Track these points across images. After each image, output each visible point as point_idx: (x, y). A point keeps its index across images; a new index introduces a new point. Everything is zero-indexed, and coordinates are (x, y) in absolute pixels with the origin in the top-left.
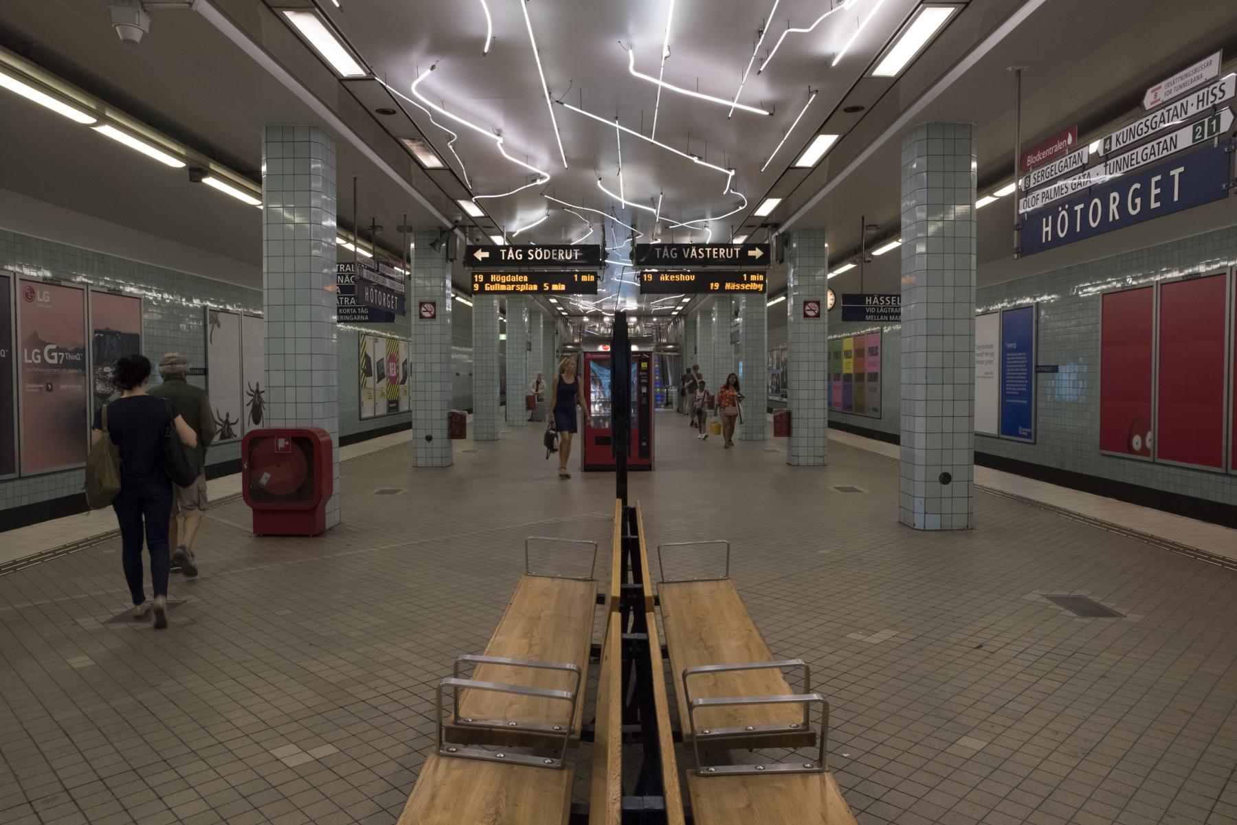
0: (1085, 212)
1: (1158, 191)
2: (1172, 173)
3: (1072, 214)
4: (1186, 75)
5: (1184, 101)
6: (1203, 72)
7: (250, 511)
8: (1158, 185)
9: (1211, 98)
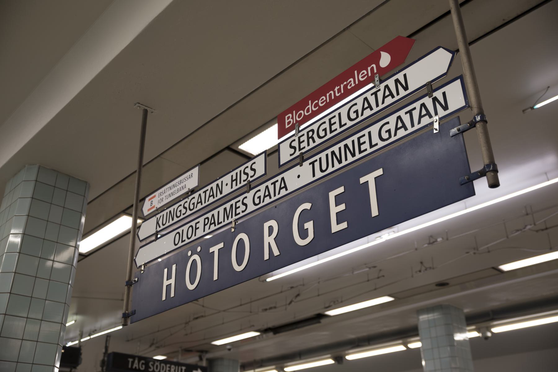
0: (225, 253)
1: (342, 207)
2: (211, 250)
3: (207, 258)
4: (174, 186)
5: (219, 182)
8: (339, 200)
9: (244, 177)
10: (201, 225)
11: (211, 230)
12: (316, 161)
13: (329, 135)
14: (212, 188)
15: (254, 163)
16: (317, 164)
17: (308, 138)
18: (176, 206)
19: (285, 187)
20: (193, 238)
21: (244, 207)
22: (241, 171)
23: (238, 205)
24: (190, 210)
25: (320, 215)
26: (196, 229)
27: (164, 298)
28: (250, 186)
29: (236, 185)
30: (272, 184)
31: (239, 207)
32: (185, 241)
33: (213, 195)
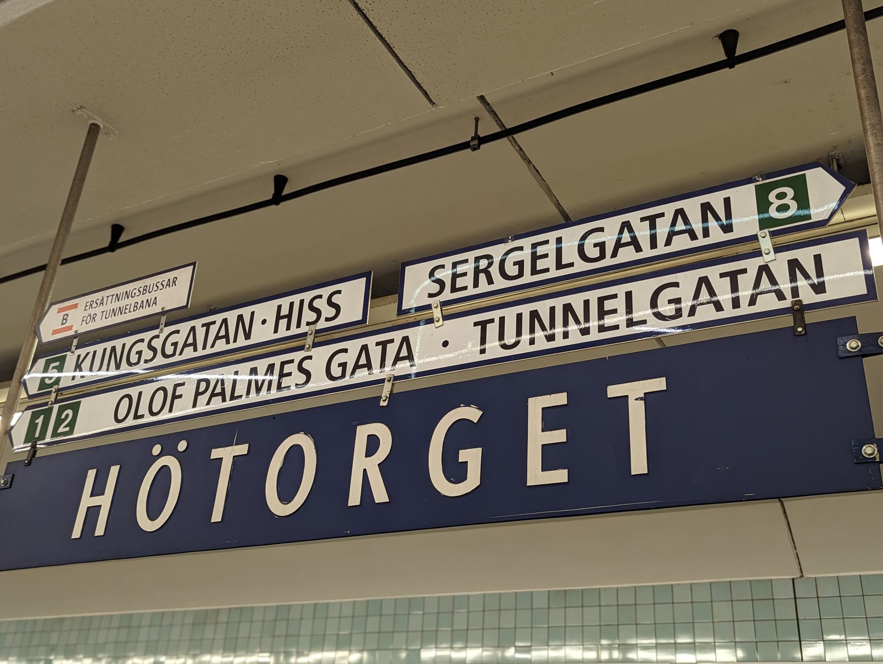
1: (559, 436)
2: (216, 453)
5: (246, 312)
6: (159, 294)
7: (41, 327)
9: (309, 316)
10: (188, 392)
11: (213, 406)
12: (492, 321)
13: (528, 278)
14: (225, 321)
15: (339, 292)
16: (493, 330)
17: (477, 271)
18: (129, 340)
19: (410, 357)
20: (165, 415)
21: (303, 378)
22: (302, 302)
23: (287, 369)
24: (165, 355)
25: (501, 438)
26: (175, 397)
27: (76, 533)
28: (323, 338)
29: (288, 328)
30: (203, 325)
31: (290, 374)
32: (142, 416)
33: (227, 337)
